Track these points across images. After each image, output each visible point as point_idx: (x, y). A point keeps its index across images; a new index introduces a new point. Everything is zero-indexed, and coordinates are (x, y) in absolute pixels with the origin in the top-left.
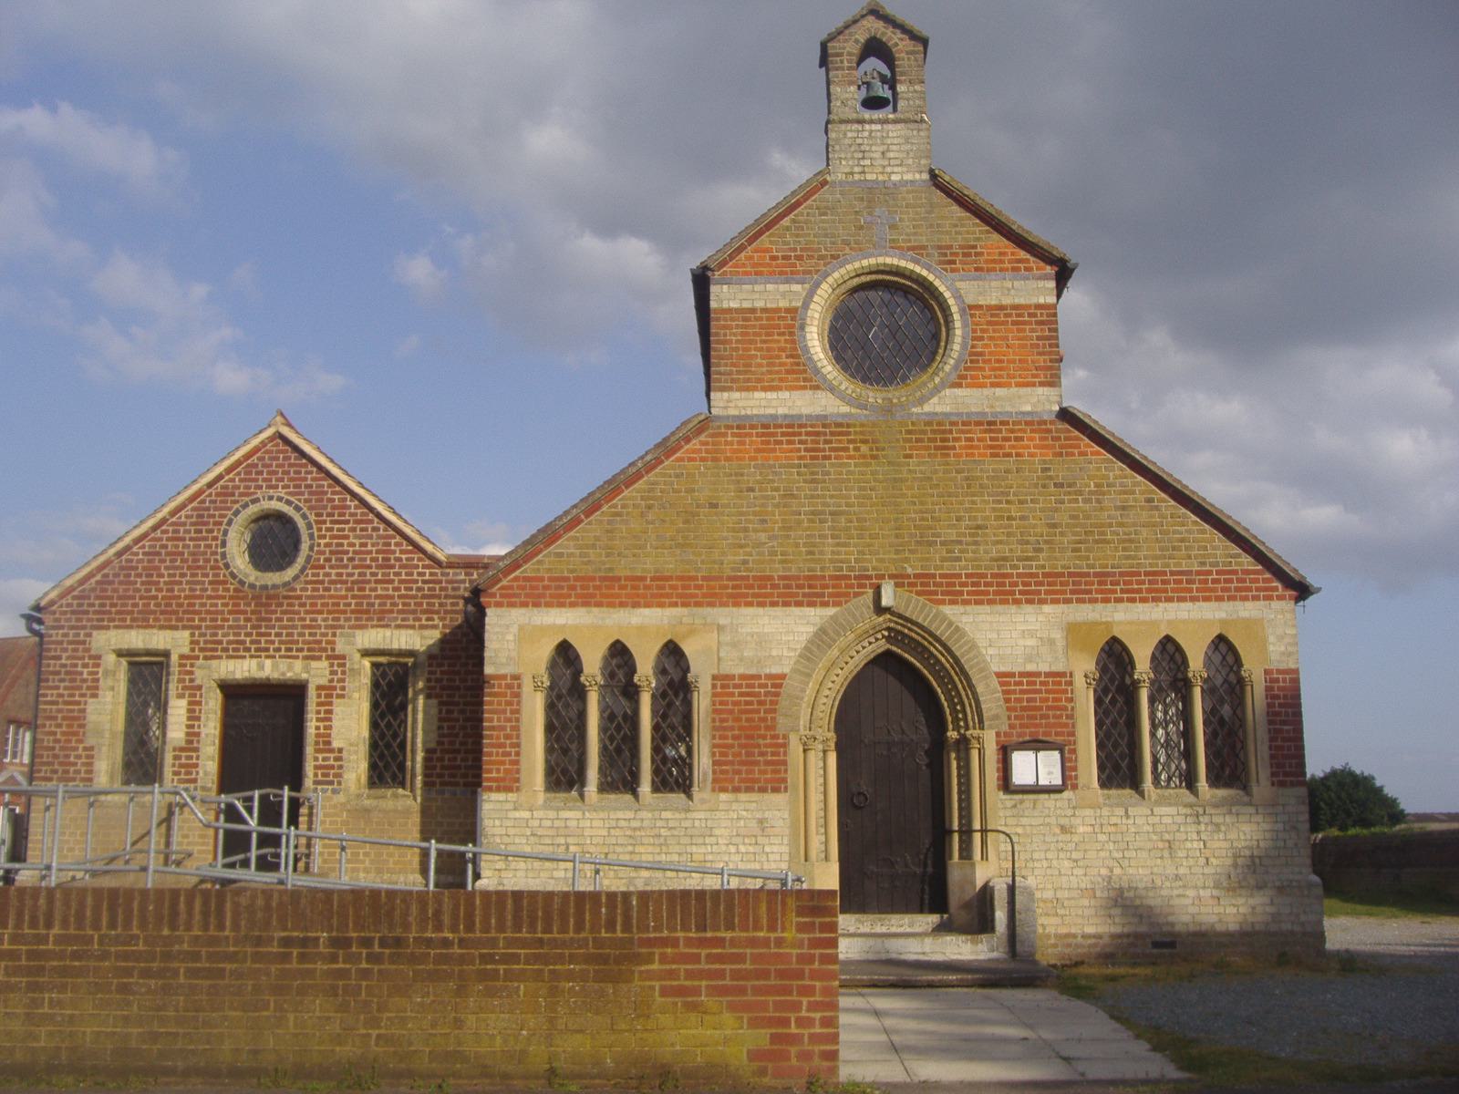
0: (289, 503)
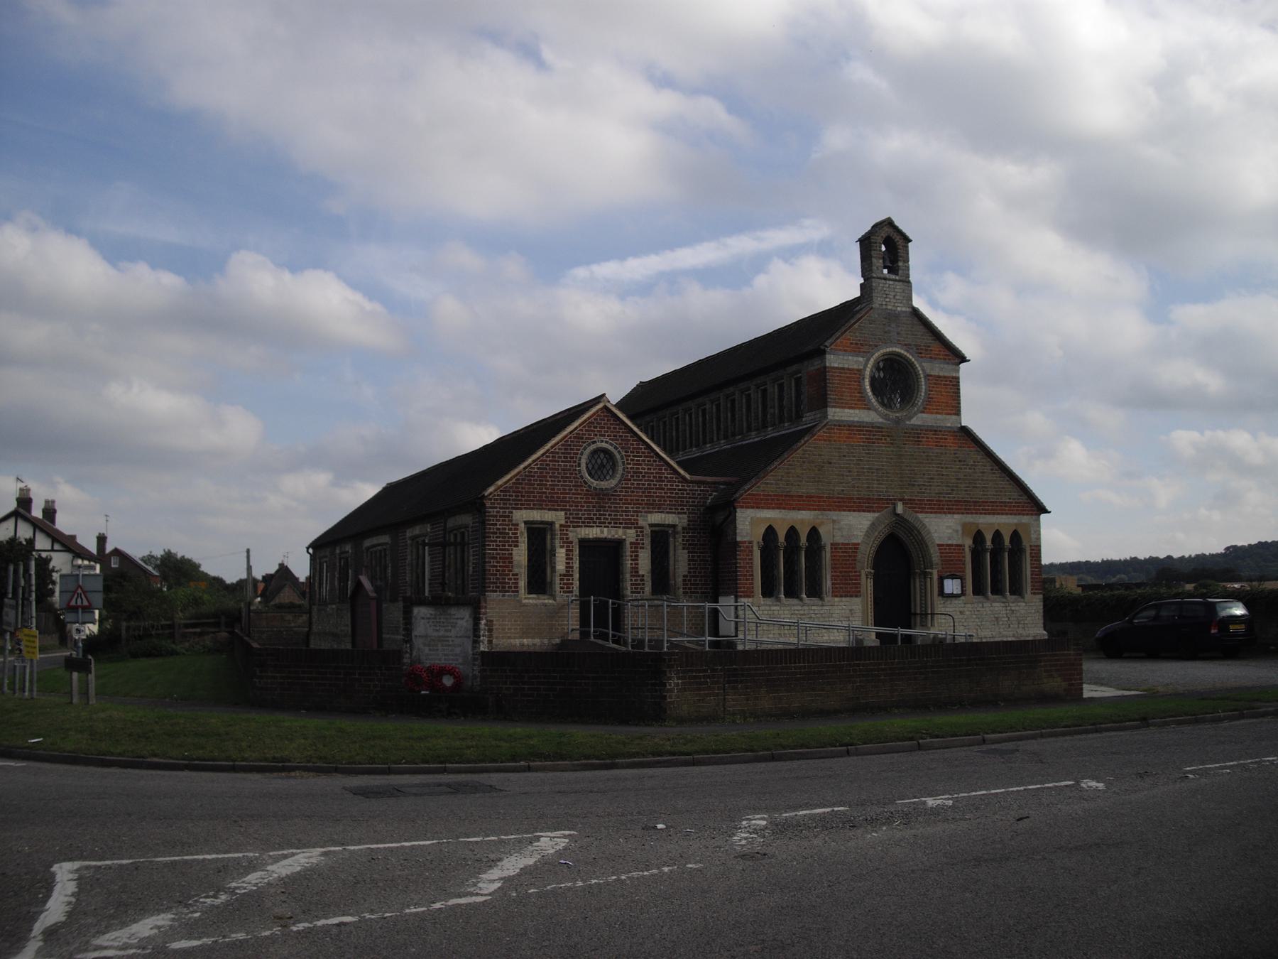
0: (611, 445)
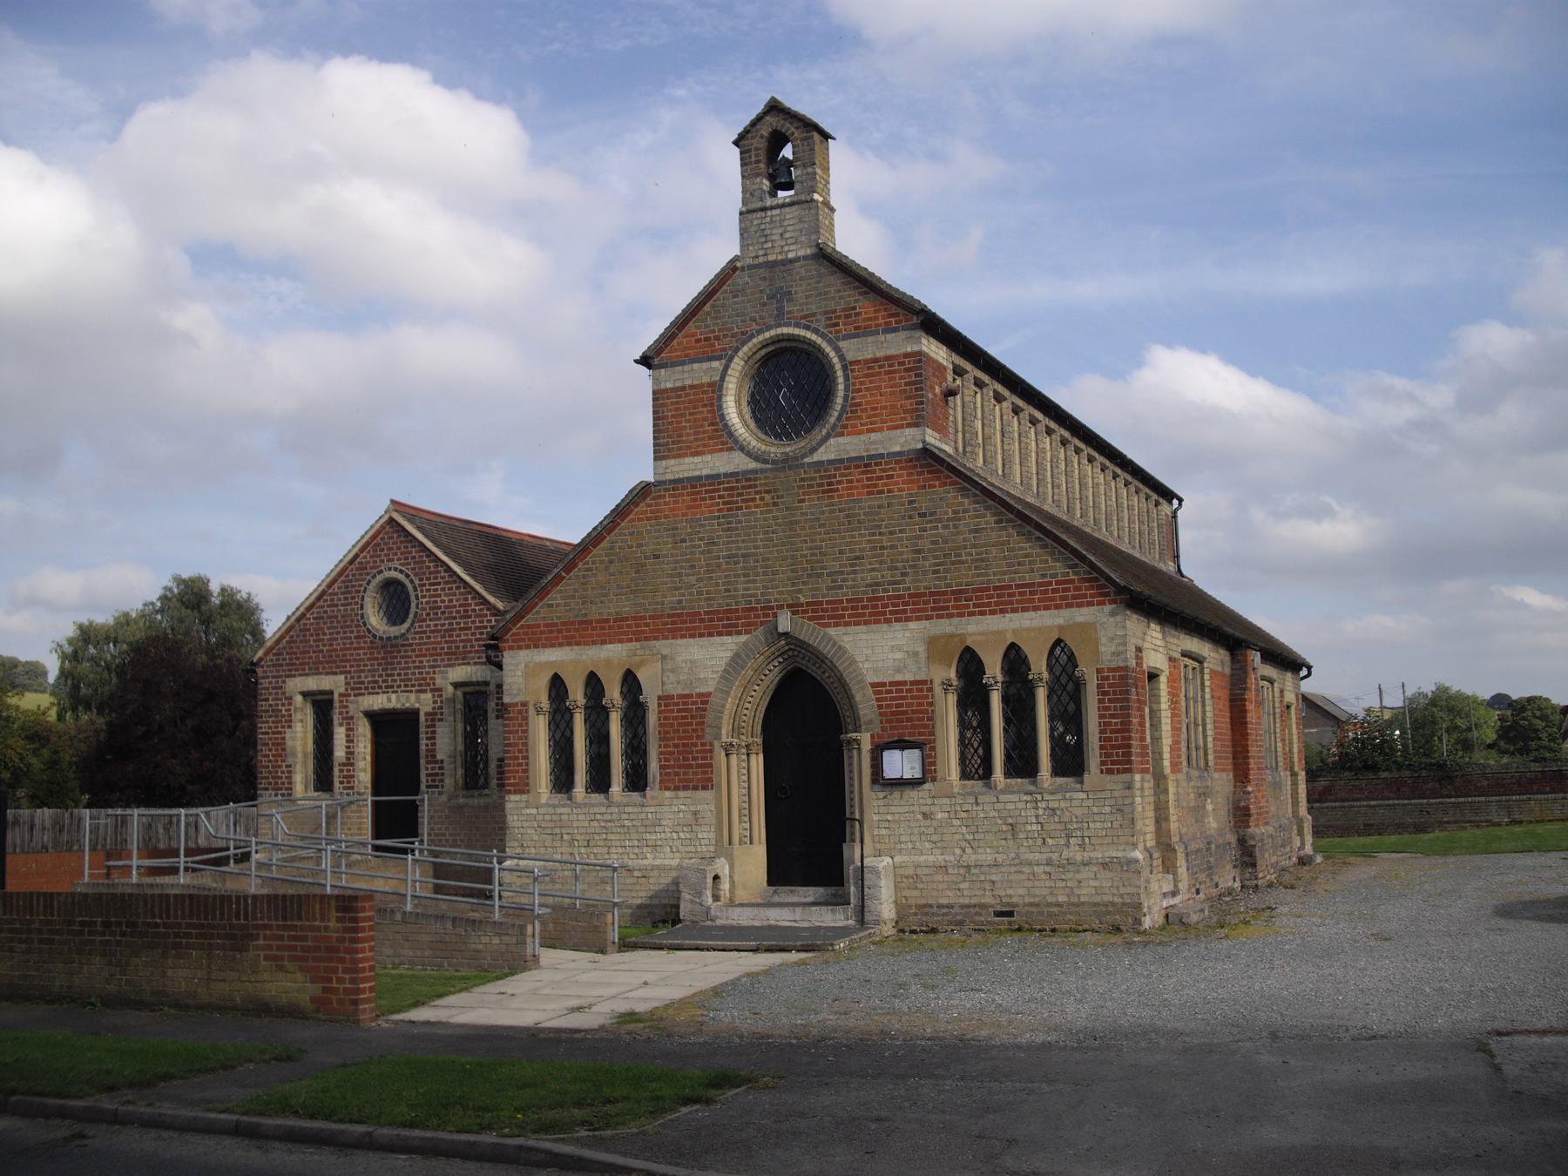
0: (401, 572)
